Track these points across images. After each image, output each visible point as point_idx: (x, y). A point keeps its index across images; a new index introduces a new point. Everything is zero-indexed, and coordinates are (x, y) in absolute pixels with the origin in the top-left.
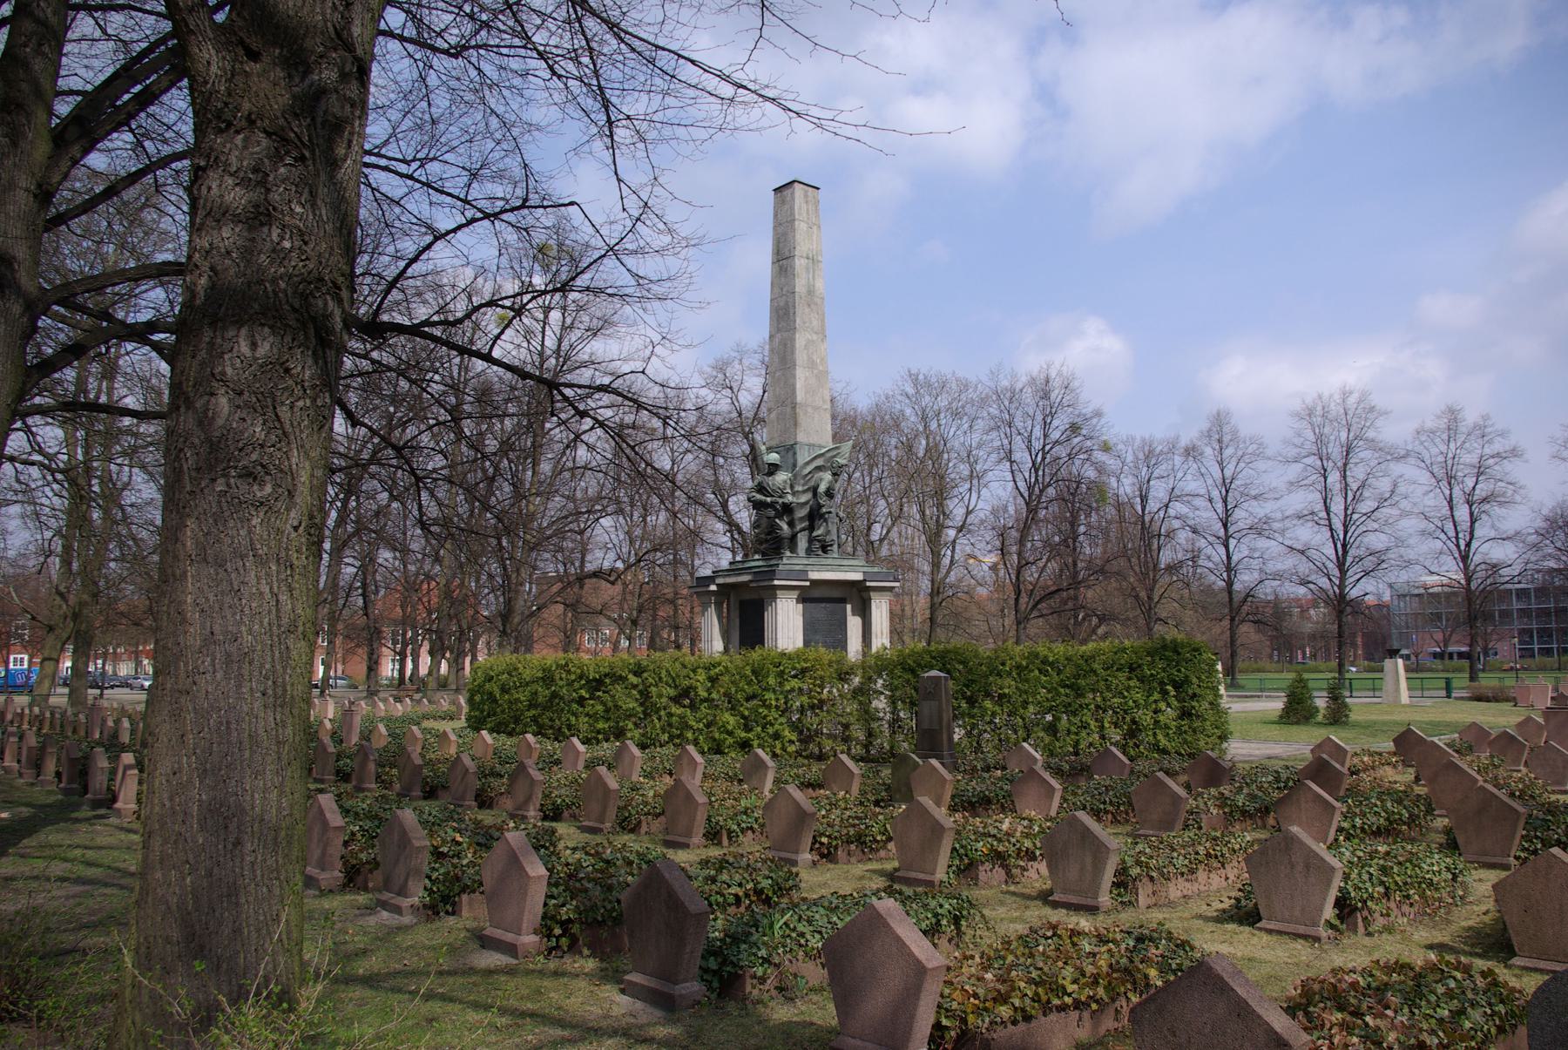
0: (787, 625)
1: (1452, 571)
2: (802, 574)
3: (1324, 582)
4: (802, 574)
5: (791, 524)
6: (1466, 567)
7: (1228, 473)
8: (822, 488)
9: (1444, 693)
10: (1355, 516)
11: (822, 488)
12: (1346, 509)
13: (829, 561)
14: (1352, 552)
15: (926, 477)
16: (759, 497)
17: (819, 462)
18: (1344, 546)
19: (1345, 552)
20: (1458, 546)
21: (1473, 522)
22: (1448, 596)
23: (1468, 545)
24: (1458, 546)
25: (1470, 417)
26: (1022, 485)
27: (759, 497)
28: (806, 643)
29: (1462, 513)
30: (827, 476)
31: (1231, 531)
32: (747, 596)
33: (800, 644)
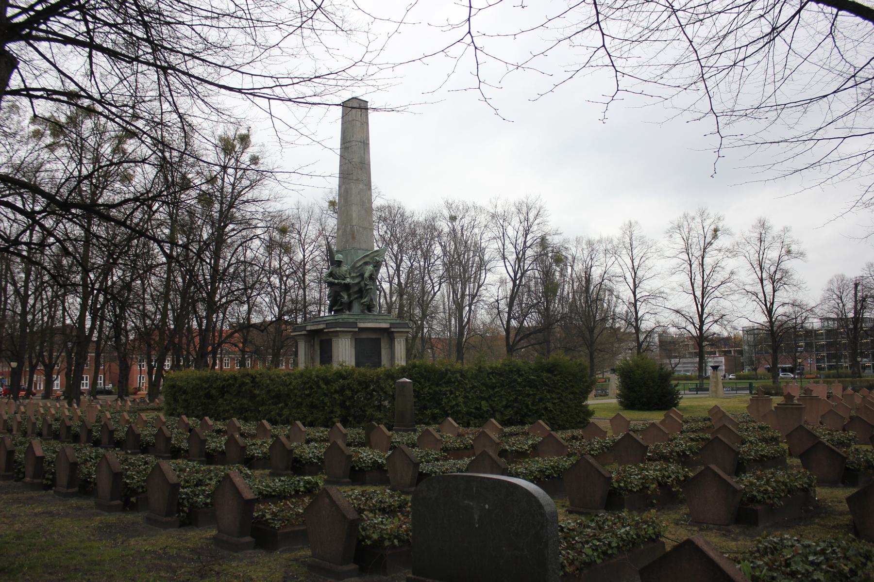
0: (344, 353)
1: (762, 319)
2: (354, 325)
3: (690, 327)
4: (354, 325)
5: (349, 296)
6: (771, 318)
7: (636, 264)
8: (367, 275)
9: (748, 392)
10: (709, 288)
11: (367, 275)
12: (703, 283)
13: (371, 317)
14: (706, 311)
15: (464, 266)
16: (331, 279)
17: (367, 259)
18: (702, 306)
19: (703, 310)
20: (766, 305)
21: (774, 291)
22: (830, 332)
23: (772, 304)
24: (766, 305)
25: (776, 228)
26: (510, 269)
27: (331, 279)
28: (358, 364)
29: (769, 288)
30: (370, 268)
31: (638, 297)
32: (324, 338)
33: (353, 363)
